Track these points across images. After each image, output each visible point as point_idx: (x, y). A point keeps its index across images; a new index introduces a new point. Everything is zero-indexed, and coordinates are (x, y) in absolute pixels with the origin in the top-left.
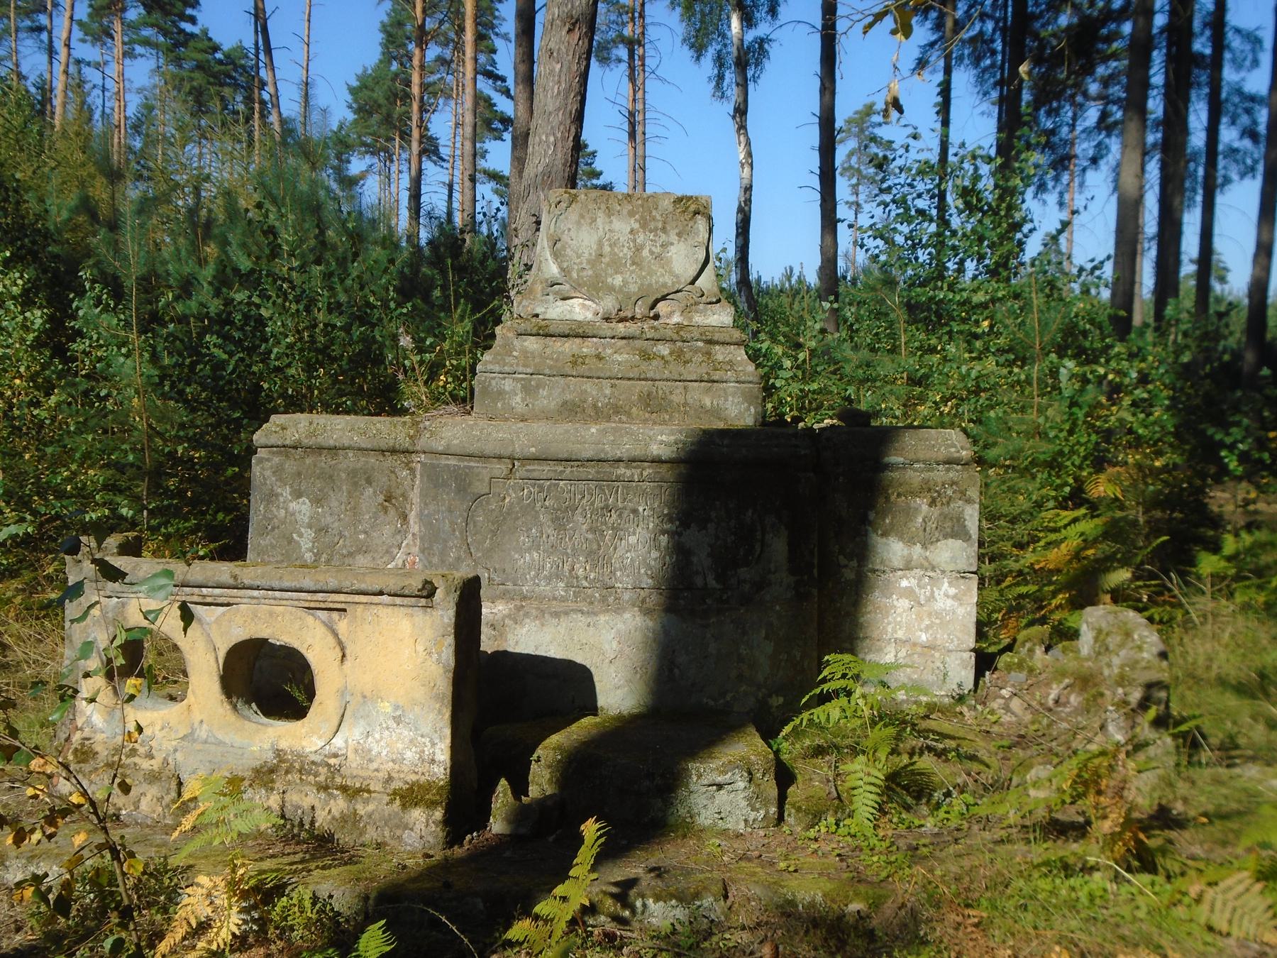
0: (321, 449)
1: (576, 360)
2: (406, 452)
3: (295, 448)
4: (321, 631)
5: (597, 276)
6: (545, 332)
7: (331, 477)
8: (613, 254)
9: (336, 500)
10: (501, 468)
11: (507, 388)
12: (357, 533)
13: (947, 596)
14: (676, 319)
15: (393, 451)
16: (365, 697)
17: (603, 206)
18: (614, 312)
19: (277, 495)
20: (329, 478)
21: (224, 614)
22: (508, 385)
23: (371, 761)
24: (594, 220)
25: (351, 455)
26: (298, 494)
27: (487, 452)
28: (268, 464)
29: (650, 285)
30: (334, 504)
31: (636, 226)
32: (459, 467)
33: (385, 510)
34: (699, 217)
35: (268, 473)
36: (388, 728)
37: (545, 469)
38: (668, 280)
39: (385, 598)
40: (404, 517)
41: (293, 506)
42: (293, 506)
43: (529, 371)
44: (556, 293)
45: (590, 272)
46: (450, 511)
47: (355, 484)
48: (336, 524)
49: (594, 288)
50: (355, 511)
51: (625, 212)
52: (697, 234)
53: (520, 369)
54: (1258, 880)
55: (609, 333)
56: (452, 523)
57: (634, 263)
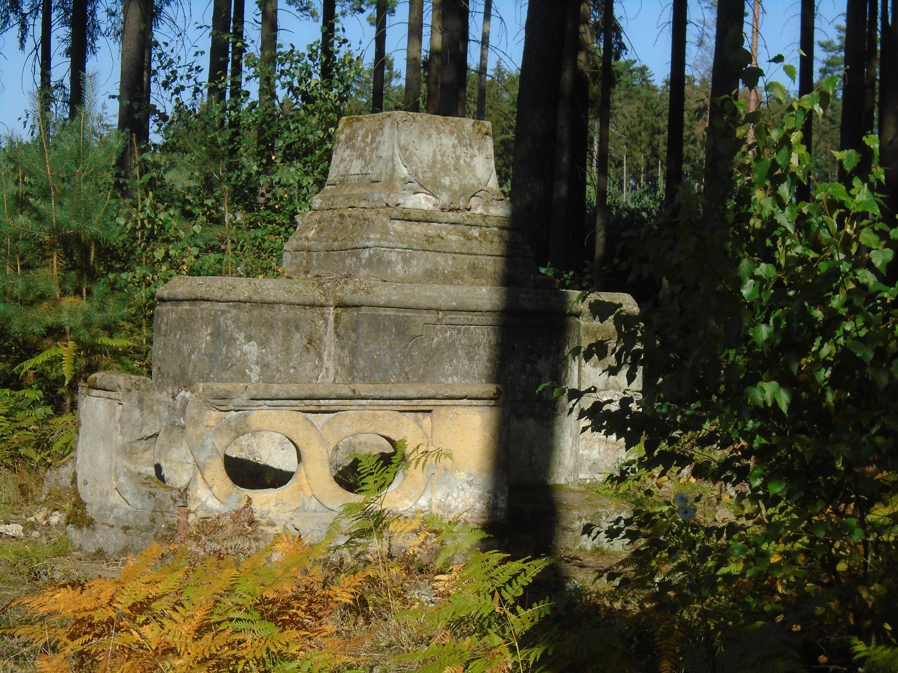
0: (264, 303)
1: (429, 239)
2: (322, 306)
3: (245, 302)
4: (412, 426)
5: (435, 177)
6: (407, 218)
7: (271, 325)
8: (443, 162)
9: (276, 343)
10: (430, 317)
11: (393, 259)
12: (289, 368)
14: (480, 210)
15: (312, 305)
16: (446, 469)
17: (434, 126)
18: (448, 204)
19: (235, 339)
20: (270, 325)
21: (334, 417)
22: (393, 256)
23: (450, 512)
24: (430, 136)
25: (283, 308)
26: (249, 339)
27: (421, 306)
28: (229, 315)
29: (465, 185)
30: (274, 346)
31: (456, 142)
32: (399, 316)
33: (308, 350)
34: (488, 137)
35: (229, 322)
36: (463, 489)
37: (461, 318)
38: (474, 181)
39: (465, 401)
40: (320, 356)
41: (246, 347)
42: (246, 347)
43: (405, 246)
44: (410, 189)
45: (430, 175)
46: (391, 349)
47: (288, 330)
48: (275, 361)
49: (431, 187)
50: (287, 351)
51: (447, 131)
52: (487, 149)
53: (400, 245)
55: (445, 220)
56: (392, 358)
57: (456, 169)
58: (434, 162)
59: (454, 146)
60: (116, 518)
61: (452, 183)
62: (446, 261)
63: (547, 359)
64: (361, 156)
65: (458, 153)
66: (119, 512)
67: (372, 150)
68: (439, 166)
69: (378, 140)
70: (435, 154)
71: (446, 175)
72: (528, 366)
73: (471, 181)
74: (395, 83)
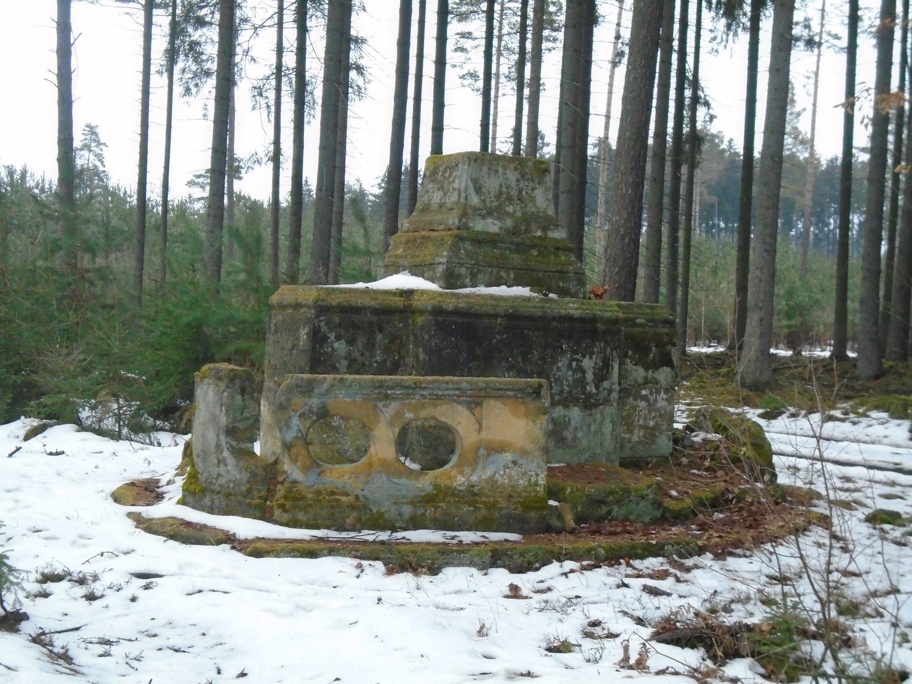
8: (508, 193)
13: (663, 399)
22: (463, 271)
26: (338, 338)
42: (336, 345)
54: (732, 611)
57: (519, 199)
58: (501, 193)
59: (518, 181)
60: (220, 486)
61: (515, 211)
62: (508, 275)
63: (591, 358)
64: (441, 188)
65: (521, 185)
66: (222, 481)
67: (449, 183)
68: (504, 196)
69: (454, 174)
70: (501, 186)
71: (510, 204)
72: (574, 364)
73: (531, 209)
74: (546, 150)
